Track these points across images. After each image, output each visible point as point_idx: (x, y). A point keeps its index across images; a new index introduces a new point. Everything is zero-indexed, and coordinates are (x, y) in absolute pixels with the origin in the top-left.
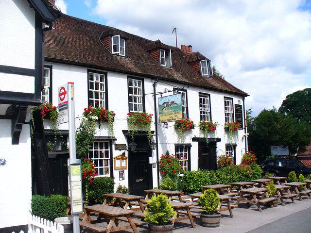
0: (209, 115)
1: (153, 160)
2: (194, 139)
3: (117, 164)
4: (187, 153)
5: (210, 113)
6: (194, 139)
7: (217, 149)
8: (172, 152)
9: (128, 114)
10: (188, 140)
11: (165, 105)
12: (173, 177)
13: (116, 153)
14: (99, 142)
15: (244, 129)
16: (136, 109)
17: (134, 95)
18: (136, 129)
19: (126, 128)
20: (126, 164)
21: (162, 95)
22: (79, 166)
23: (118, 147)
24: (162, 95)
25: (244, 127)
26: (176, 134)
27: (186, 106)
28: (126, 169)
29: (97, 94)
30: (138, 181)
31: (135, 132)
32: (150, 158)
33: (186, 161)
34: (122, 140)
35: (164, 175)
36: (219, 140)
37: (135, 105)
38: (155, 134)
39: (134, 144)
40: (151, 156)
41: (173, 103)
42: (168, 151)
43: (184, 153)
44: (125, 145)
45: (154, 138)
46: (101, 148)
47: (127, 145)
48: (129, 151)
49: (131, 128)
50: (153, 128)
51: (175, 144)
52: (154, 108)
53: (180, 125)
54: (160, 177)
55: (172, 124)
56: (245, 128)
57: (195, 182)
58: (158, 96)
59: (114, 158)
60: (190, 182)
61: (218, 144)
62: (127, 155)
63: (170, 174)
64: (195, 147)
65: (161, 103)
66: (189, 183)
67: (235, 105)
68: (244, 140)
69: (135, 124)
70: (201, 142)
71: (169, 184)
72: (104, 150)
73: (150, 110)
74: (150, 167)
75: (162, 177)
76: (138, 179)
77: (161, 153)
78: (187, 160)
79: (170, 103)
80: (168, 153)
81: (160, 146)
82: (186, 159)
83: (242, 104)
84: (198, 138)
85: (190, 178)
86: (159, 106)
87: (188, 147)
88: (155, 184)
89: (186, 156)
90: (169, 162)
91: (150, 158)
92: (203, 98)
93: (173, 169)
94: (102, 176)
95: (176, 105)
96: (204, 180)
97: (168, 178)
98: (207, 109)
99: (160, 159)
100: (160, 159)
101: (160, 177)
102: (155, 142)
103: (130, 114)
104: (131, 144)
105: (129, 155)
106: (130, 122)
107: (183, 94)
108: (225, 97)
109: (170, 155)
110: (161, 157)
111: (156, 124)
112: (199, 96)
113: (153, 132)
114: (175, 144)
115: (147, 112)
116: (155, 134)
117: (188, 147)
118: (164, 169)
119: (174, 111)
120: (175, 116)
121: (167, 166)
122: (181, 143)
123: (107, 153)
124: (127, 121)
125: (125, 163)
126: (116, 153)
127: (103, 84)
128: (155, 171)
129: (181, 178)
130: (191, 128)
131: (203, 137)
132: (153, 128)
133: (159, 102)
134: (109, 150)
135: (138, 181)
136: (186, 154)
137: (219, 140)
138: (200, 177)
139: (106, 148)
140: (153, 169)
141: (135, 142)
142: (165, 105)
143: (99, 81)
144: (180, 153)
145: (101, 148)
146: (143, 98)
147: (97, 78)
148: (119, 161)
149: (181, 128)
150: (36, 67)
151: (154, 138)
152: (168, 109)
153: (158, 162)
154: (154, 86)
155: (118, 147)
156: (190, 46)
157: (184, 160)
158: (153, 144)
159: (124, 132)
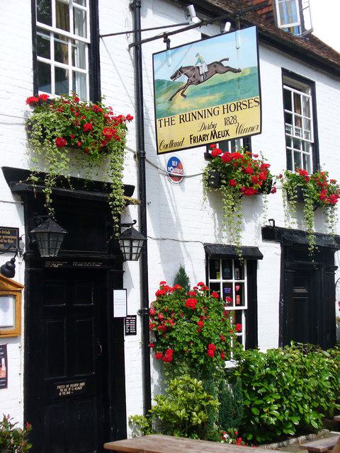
0: (310, 153)
1: (126, 303)
2: (270, 233)
4: (245, 281)
5: (315, 146)
6: (270, 233)
8: (197, 274)
9: (30, 102)
10: (249, 237)
11: (184, 79)
12: (204, 372)
16: (62, 89)
18: (63, 167)
19: (21, 158)
20: (17, 317)
21: (167, 41)
24: (167, 41)
26: (211, 210)
27: (298, 23)
28: (14, 337)
30: (64, 390)
31: (61, 181)
32: (118, 295)
33: (238, 313)
35: (170, 364)
37: (61, 74)
38: (135, 196)
39: (54, 227)
40: (120, 287)
41: (217, 67)
42: (182, 271)
43: (233, 281)
44: (14, 231)
45: (133, 212)
47: (22, 233)
48: (33, 261)
49: (43, 158)
50: (129, 176)
51: (207, 247)
52: (134, 100)
53: (228, 171)
54: (155, 375)
55: (195, 162)
57: (286, 393)
58: (147, 49)
60: (268, 393)
62: (20, 277)
63: (196, 361)
64: (272, 254)
65: (165, 74)
66: (261, 397)
69: (60, 146)
71: (192, 402)
73: (118, 99)
74: (118, 328)
75: (161, 372)
76: (64, 382)
77: (159, 275)
78: (246, 307)
79: (204, 70)
80: (182, 279)
81: (153, 248)
82: (241, 304)
84: (282, 230)
85: (268, 378)
86: (158, 84)
88: (134, 406)
89: (240, 293)
90: (189, 312)
92: (293, 91)
93: (207, 341)
95: (230, 76)
96: (313, 383)
97: (186, 377)
98: (305, 136)
99: (152, 298)
100: (152, 298)
101: (155, 375)
102: (136, 227)
103: (37, 103)
104: (41, 228)
105: (29, 275)
106: (38, 134)
109: (193, 284)
110: (158, 294)
111: (141, 157)
112: (283, 84)
113: (129, 190)
114: (207, 247)
115: (105, 103)
116: (135, 196)
117: (252, 257)
118: (172, 339)
119: (223, 100)
120: (227, 122)
121: (183, 329)
122: (225, 242)
124: (22, 133)
128: (133, 347)
129: (229, 374)
130: (261, 191)
131: (295, 227)
132: (129, 176)
133: (158, 68)
135: (64, 390)
136: (241, 285)
138: (303, 373)
140: (127, 338)
141: (60, 220)
142: (184, 79)
144: (221, 280)
149: (231, 184)
150: (123, 341)
151: (133, 212)
152: (195, 94)
153: (145, 313)
157: (234, 308)
158: (129, 236)
159: (13, 175)
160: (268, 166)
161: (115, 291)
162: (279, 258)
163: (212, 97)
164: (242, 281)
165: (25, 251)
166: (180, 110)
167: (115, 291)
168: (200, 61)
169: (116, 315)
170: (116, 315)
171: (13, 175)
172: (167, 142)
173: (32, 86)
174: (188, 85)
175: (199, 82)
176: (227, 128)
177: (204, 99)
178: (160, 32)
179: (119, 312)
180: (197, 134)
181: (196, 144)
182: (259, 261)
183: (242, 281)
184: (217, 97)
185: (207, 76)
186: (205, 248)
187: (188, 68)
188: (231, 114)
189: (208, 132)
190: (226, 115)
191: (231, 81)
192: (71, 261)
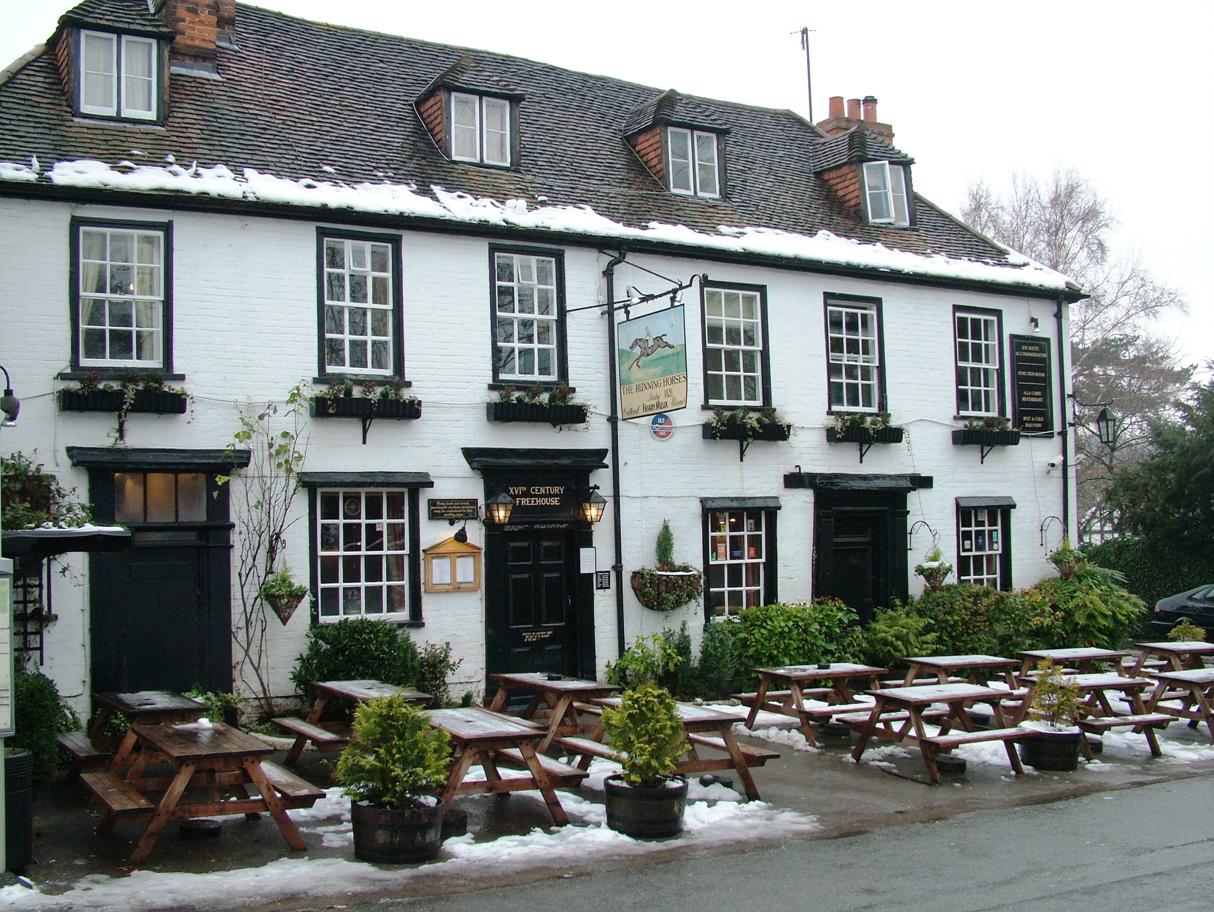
2: (794, 481)
3: (438, 572)
6: (794, 481)
7: (910, 520)
9: (491, 388)
11: (637, 350)
13: (434, 533)
14: (363, 492)
15: (1057, 440)
17: (517, 314)
21: (627, 313)
22: (7, 580)
23: (442, 511)
24: (627, 313)
25: (1057, 427)
29: (977, 348)
34: (457, 482)
36: (926, 482)
40: (589, 543)
42: (666, 528)
44: (474, 502)
46: (374, 512)
47: (481, 502)
48: (490, 525)
56: (1063, 434)
58: (620, 316)
59: (424, 551)
61: (916, 501)
67: (1013, 337)
68: (1058, 473)
70: (829, 494)
72: (383, 523)
78: (763, 560)
79: (651, 343)
83: (1046, 329)
87: (765, 514)
91: (584, 552)
94: (373, 617)
107: (749, 300)
108: (828, 296)
114: (703, 501)
117: (765, 514)
119: (664, 372)
123: (396, 533)
125: (469, 570)
126: (434, 533)
127: (872, 316)
134: (406, 521)
137: (926, 482)
139: (395, 511)
143: (369, 267)
145: (374, 512)
146: (561, 323)
147: (360, 262)
148: (446, 563)
152: (646, 365)
154: (608, 274)
155: (442, 511)
156: (870, 101)
159: (470, 454)
160: (52, 618)
161: (582, 550)
162: (811, 506)
163: (657, 370)
164: (758, 533)
165: (484, 517)
166: (636, 380)
167: (582, 550)
168: (648, 334)
169: (584, 570)
170: (584, 570)
171: (470, 454)
172: (628, 410)
173: (491, 373)
174: (641, 356)
175: (648, 355)
176: (666, 400)
177: (652, 371)
178: (621, 304)
179: (587, 566)
180: (647, 404)
181: (646, 413)
182: (778, 511)
183: (758, 533)
184: (658, 370)
185: (653, 349)
186: (701, 502)
187: (640, 340)
188: (669, 387)
189: (654, 402)
190: (666, 388)
191: (669, 356)
192: (532, 524)
